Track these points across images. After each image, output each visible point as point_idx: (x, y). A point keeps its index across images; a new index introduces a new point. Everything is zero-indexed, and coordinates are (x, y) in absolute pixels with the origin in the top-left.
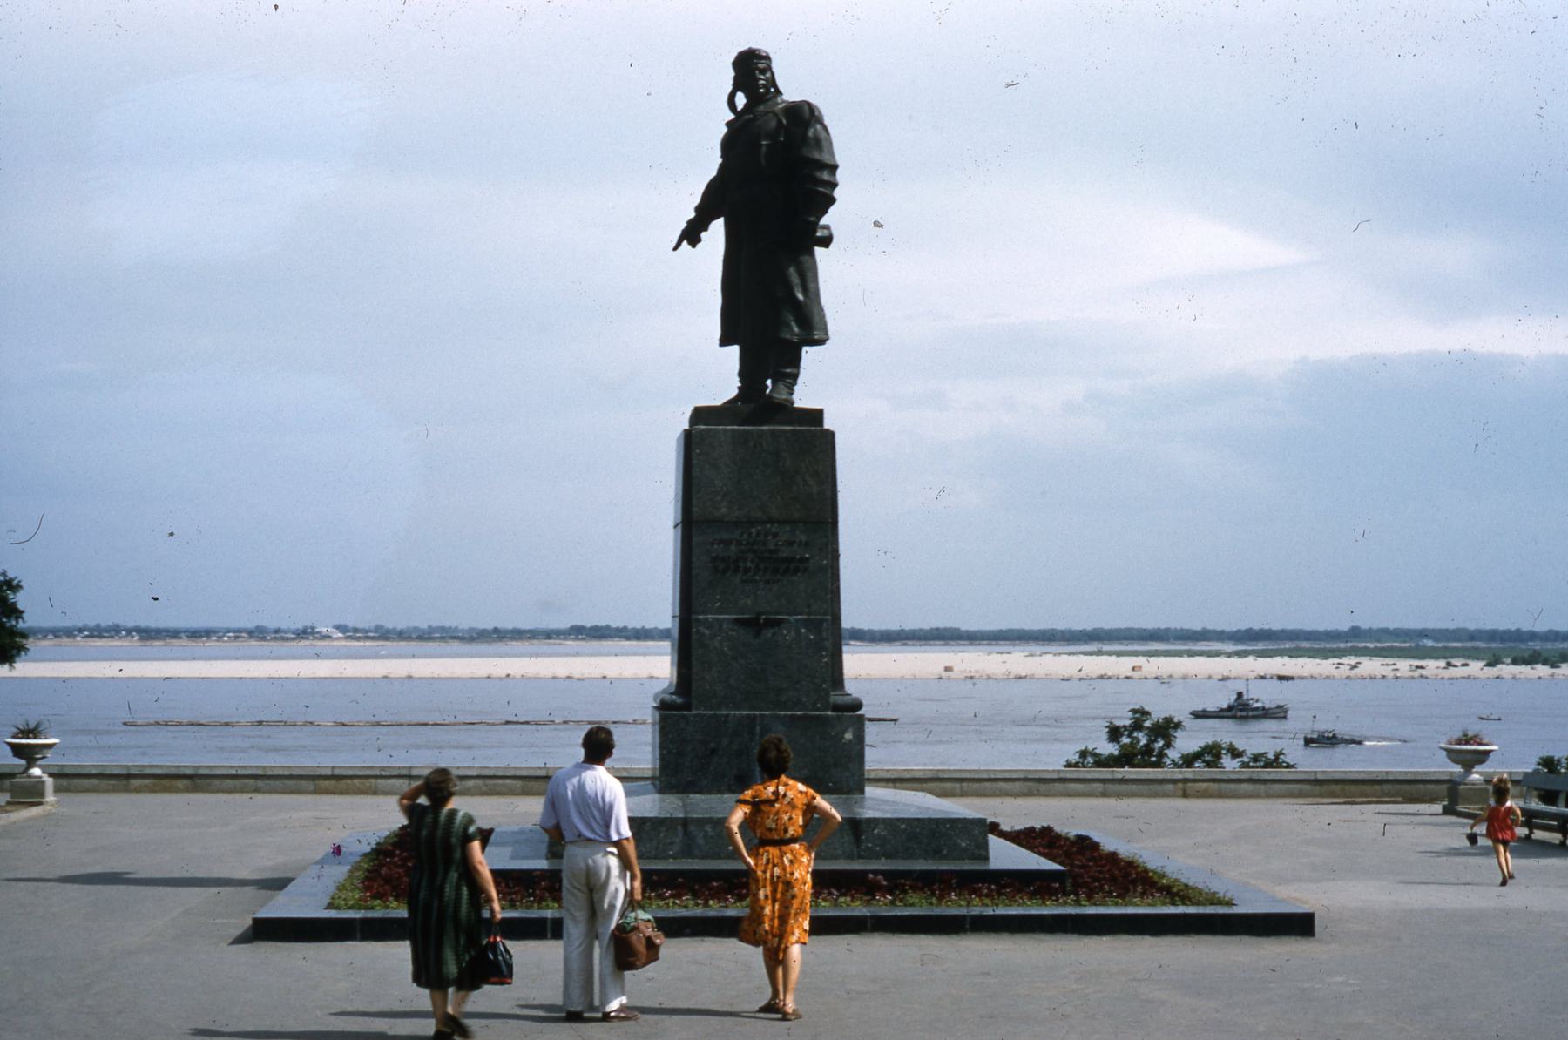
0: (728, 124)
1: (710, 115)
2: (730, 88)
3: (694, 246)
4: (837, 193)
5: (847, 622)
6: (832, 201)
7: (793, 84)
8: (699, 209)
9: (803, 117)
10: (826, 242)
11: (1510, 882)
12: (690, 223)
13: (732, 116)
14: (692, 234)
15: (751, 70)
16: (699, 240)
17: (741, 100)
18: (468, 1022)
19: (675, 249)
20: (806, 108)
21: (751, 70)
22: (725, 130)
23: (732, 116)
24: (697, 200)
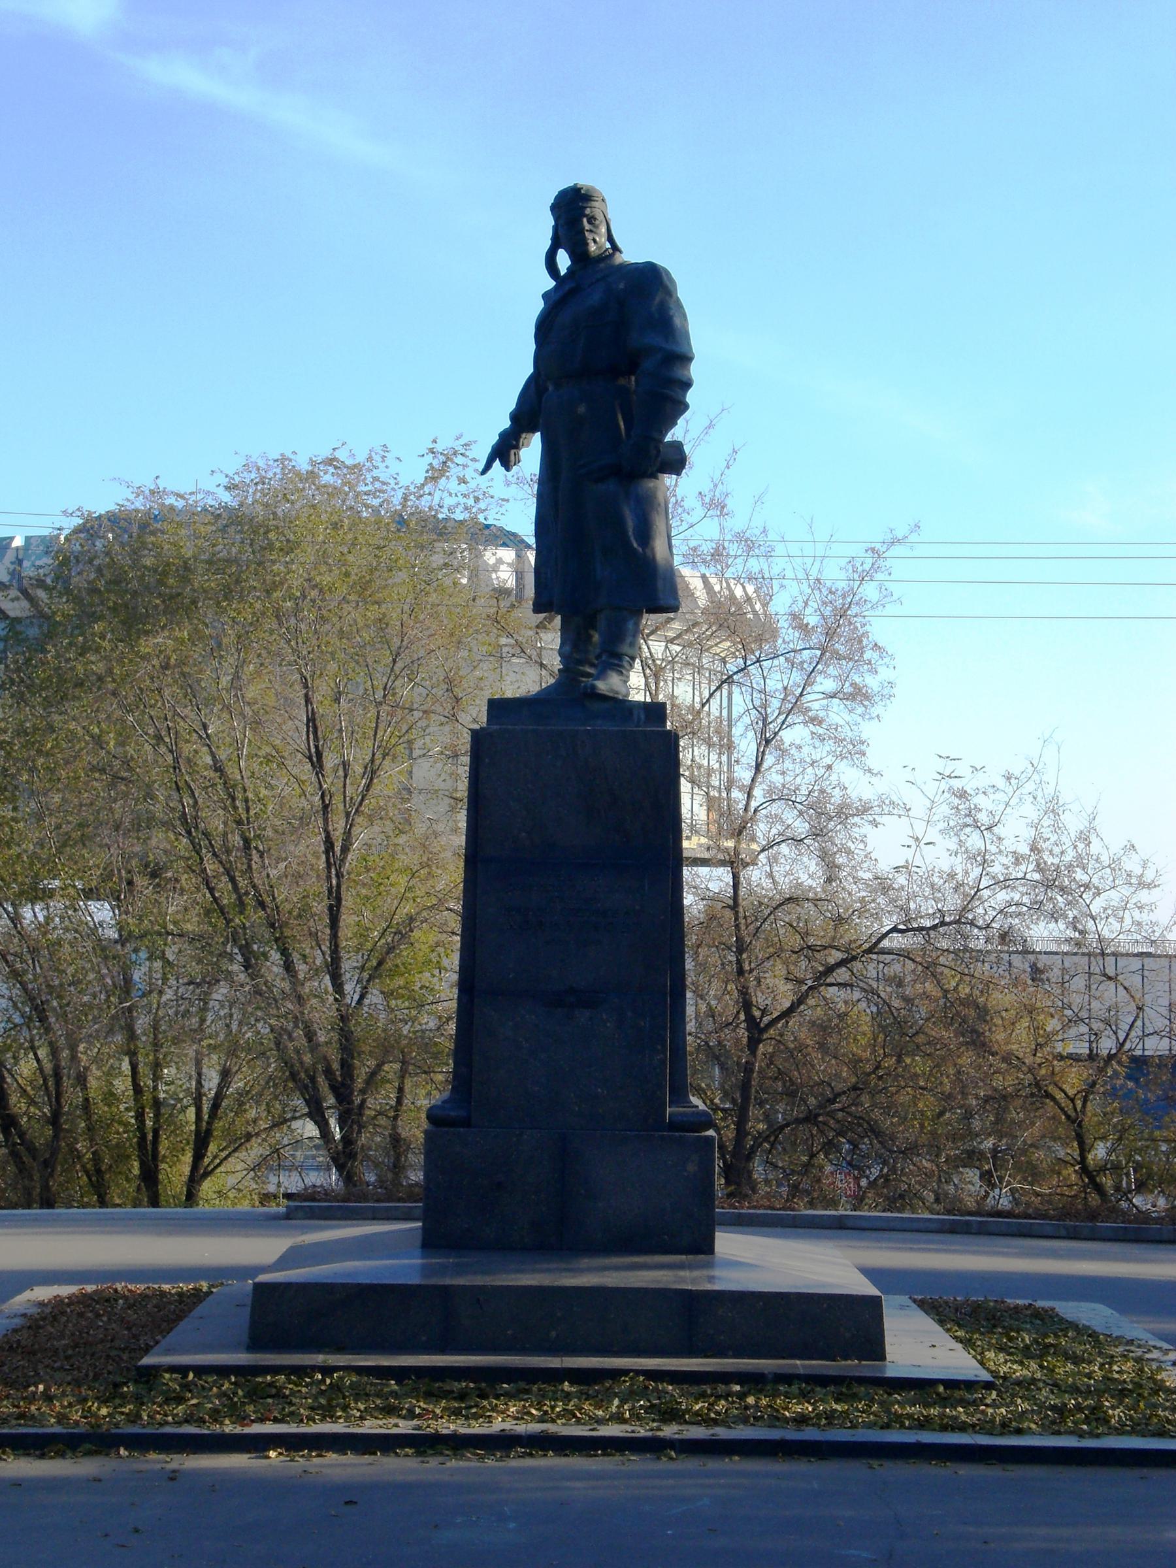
0: (546, 296)
1: (523, 283)
2: (548, 244)
9: (650, 283)
13: (551, 284)
14: (504, 451)
15: (573, 211)
21: (573, 211)
22: (540, 305)
23: (551, 284)
24: (512, 405)
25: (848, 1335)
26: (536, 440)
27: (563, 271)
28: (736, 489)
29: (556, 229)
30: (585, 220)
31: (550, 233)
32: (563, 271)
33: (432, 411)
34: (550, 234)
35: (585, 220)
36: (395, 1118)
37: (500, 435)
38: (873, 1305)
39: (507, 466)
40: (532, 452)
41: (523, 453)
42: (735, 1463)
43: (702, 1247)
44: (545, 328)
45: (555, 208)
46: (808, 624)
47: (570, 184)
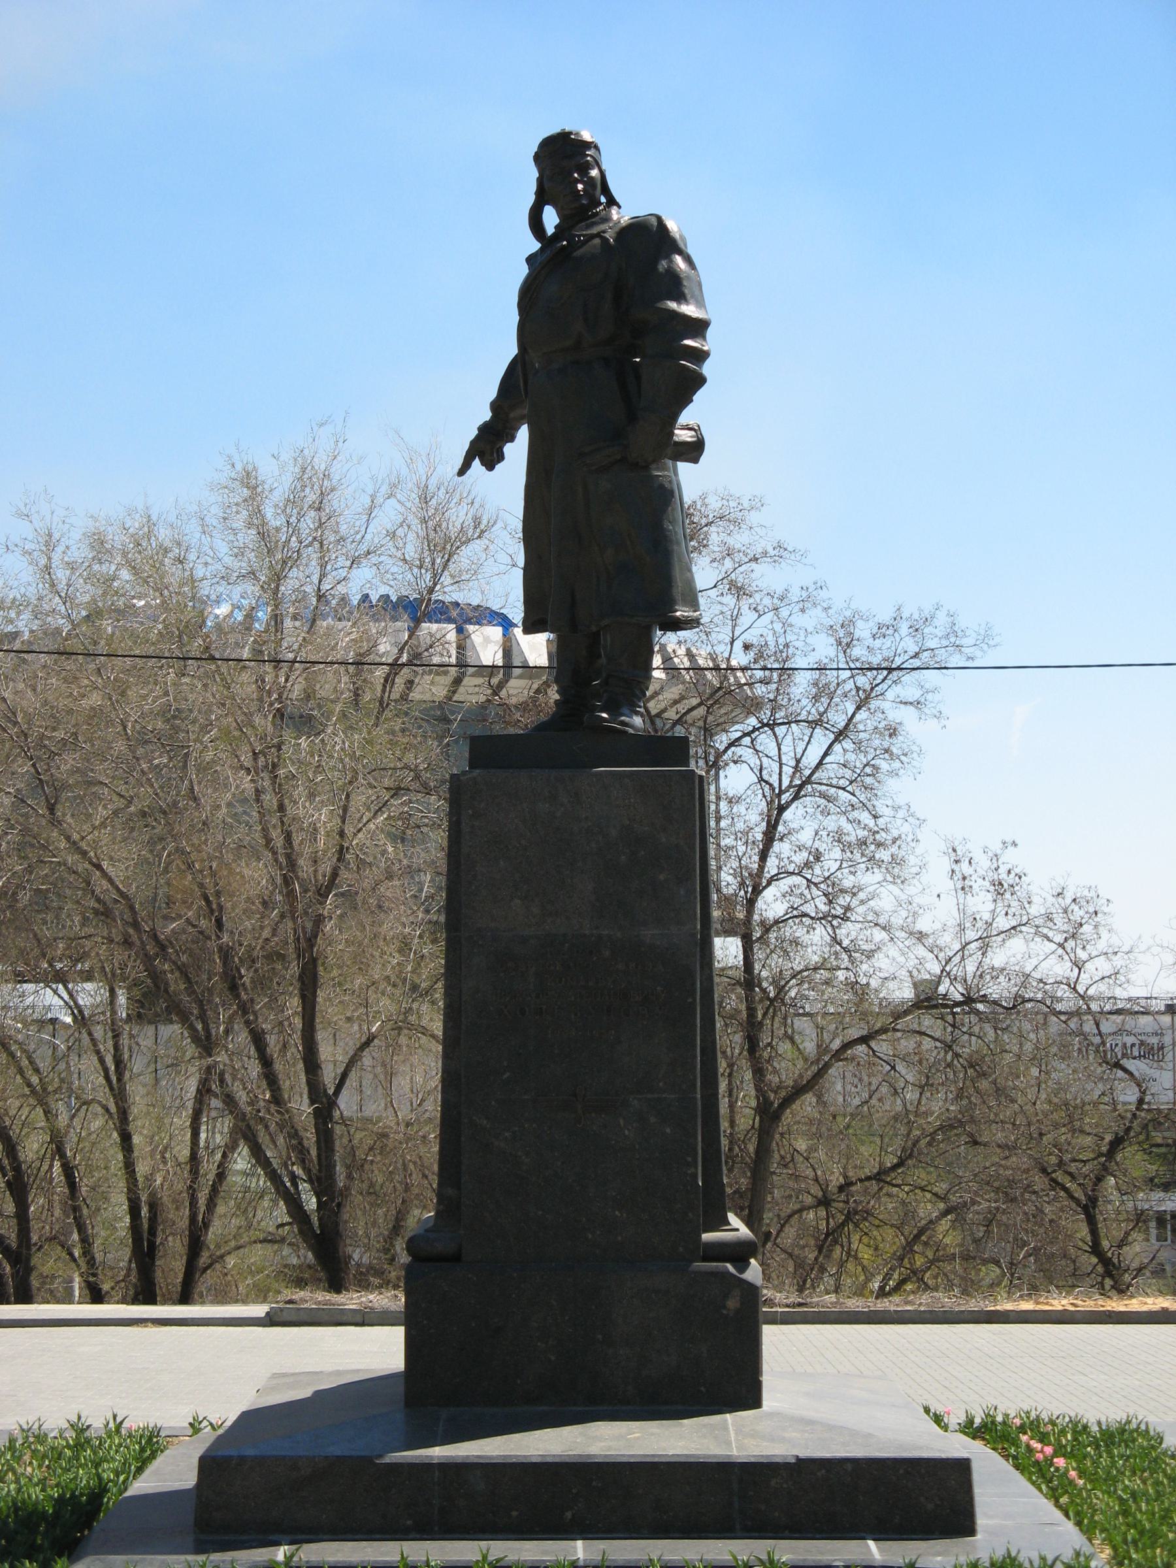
0: (530, 260)
1: (504, 248)
2: (531, 199)
3: (490, 466)
4: (707, 369)
5: (400, 1331)
6: (700, 381)
7: (636, 190)
8: (496, 406)
9: (652, 240)
10: (694, 451)
11: (1009, 840)
12: (484, 429)
13: (536, 246)
14: (487, 448)
15: (565, 165)
16: (501, 457)
17: (551, 219)
18: (294, 1547)
19: (462, 472)
20: (654, 222)
21: (565, 165)
22: (524, 270)
23: (536, 246)
24: (493, 393)
25: (930, 1506)
26: (523, 434)
27: (550, 230)
28: (749, 456)
29: (540, 181)
31: (533, 187)
32: (550, 230)
33: (387, 429)
34: (534, 188)
37: (479, 429)
38: (962, 1467)
40: (517, 450)
43: (741, 1389)
44: (529, 297)
45: (537, 158)
47: (554, 130)
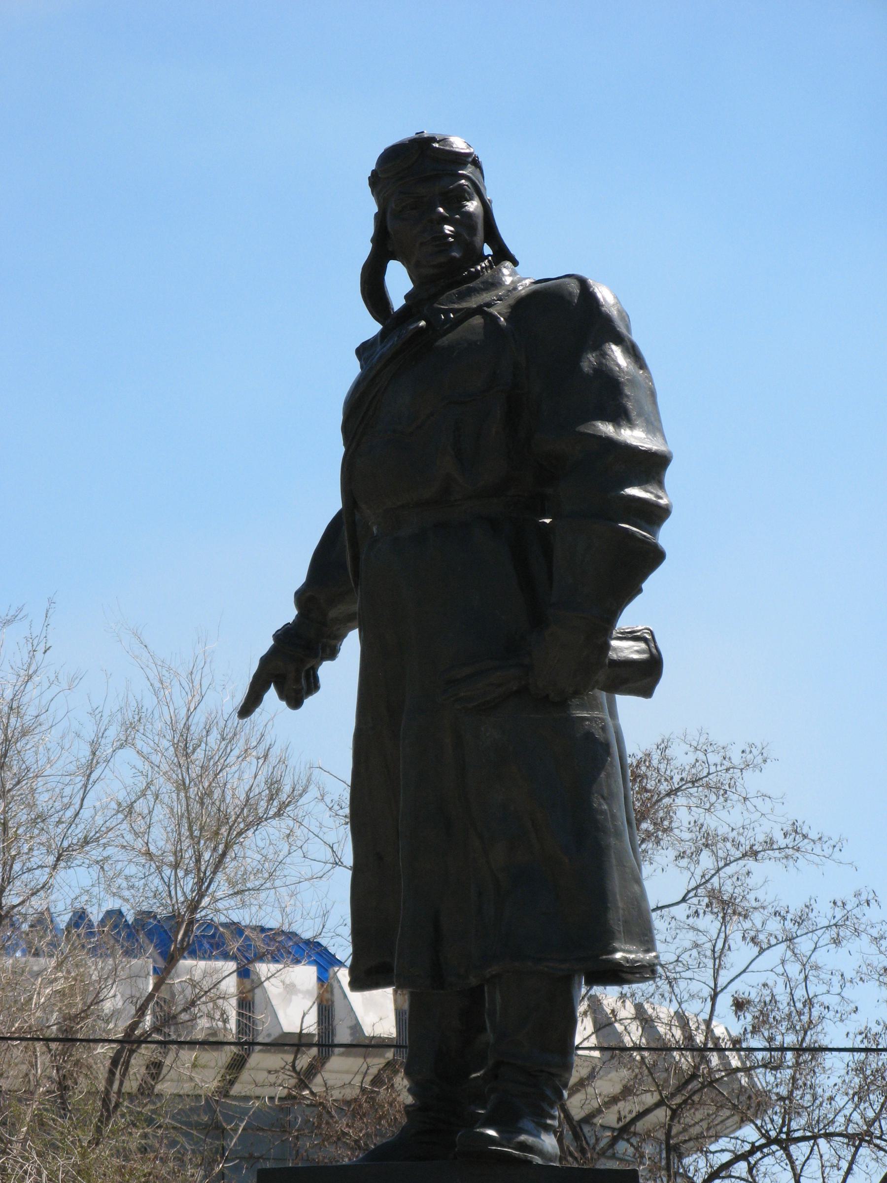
0: (364, 351)
2: (366, 249)
13: (373, 328)
14: (289, 668)
15: (423, 194)
21: (423, 194)
22: (351, 370)
23: (373, 328)
24: (299, 576)
26: (351, 645)
27: (397, 301)
29: (381, 220)
30: (486, 309)
31: (369, 229)
32: (397, 301)
35: (486, 309)
36: (823, 1166)
39: (295, 700)
40: (341, 674)
41: (326, 670)
42: (736, 980)
44: (362, 415)
46: (80, 917)
47: (403, 133)
